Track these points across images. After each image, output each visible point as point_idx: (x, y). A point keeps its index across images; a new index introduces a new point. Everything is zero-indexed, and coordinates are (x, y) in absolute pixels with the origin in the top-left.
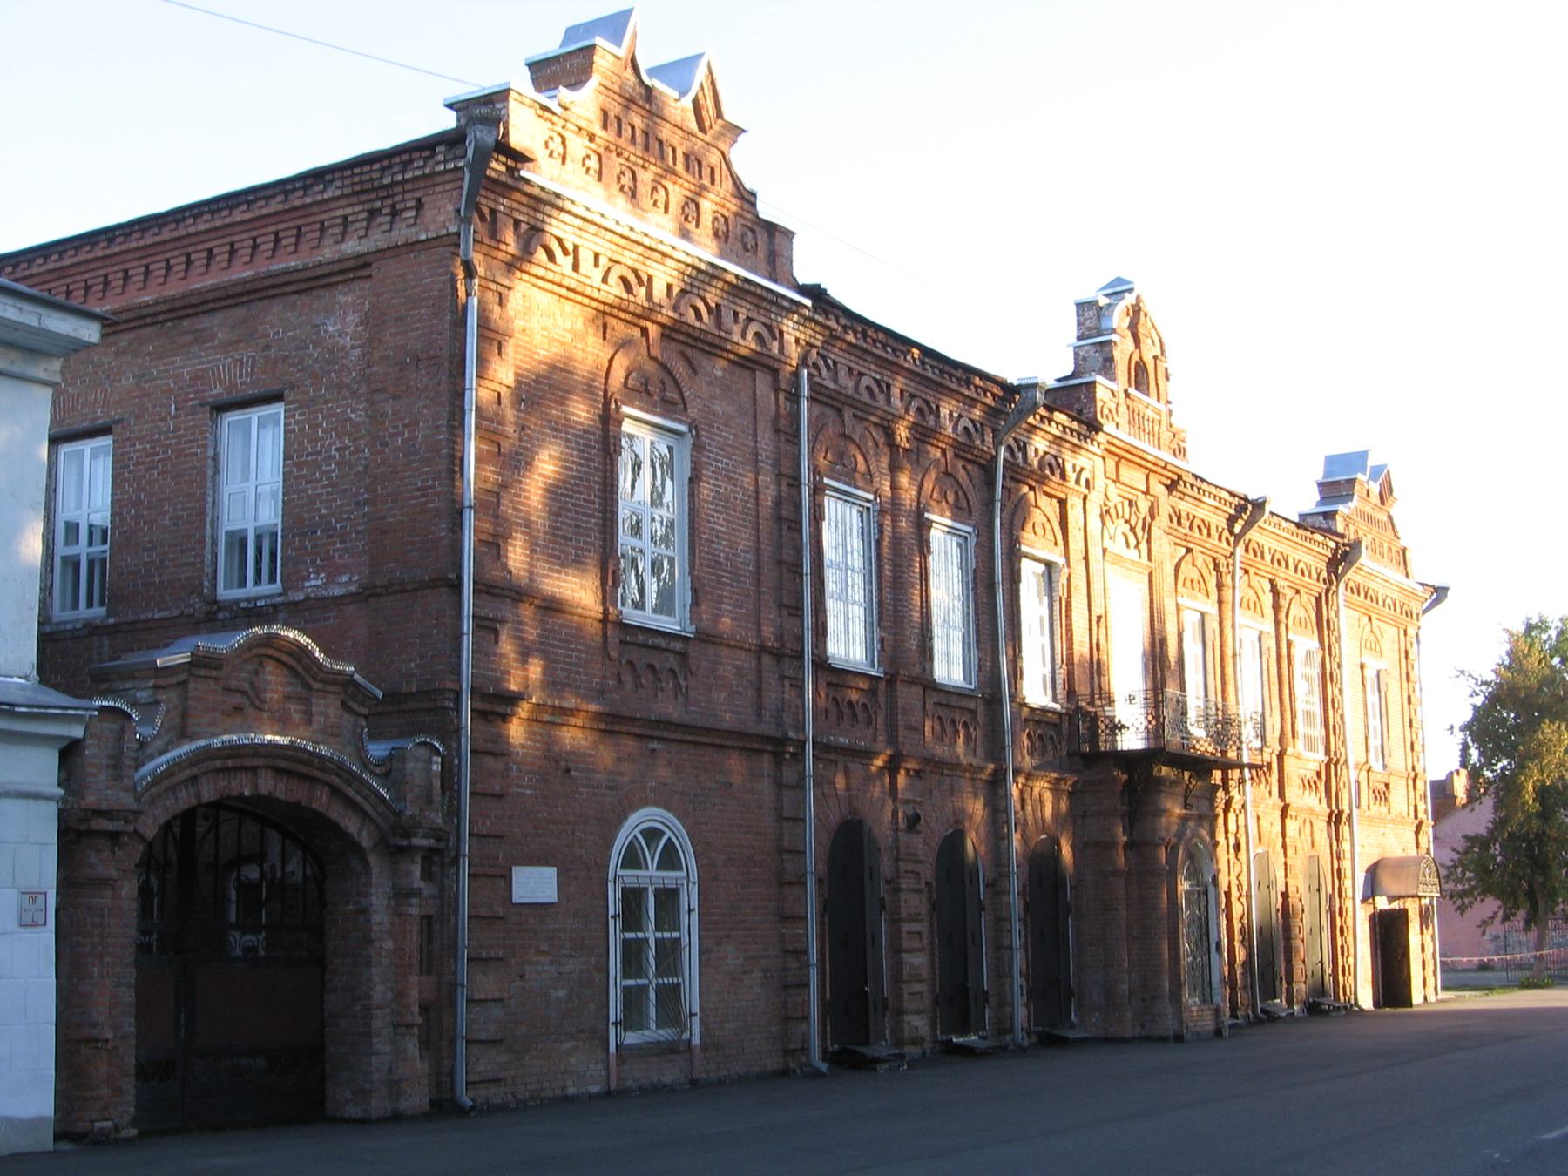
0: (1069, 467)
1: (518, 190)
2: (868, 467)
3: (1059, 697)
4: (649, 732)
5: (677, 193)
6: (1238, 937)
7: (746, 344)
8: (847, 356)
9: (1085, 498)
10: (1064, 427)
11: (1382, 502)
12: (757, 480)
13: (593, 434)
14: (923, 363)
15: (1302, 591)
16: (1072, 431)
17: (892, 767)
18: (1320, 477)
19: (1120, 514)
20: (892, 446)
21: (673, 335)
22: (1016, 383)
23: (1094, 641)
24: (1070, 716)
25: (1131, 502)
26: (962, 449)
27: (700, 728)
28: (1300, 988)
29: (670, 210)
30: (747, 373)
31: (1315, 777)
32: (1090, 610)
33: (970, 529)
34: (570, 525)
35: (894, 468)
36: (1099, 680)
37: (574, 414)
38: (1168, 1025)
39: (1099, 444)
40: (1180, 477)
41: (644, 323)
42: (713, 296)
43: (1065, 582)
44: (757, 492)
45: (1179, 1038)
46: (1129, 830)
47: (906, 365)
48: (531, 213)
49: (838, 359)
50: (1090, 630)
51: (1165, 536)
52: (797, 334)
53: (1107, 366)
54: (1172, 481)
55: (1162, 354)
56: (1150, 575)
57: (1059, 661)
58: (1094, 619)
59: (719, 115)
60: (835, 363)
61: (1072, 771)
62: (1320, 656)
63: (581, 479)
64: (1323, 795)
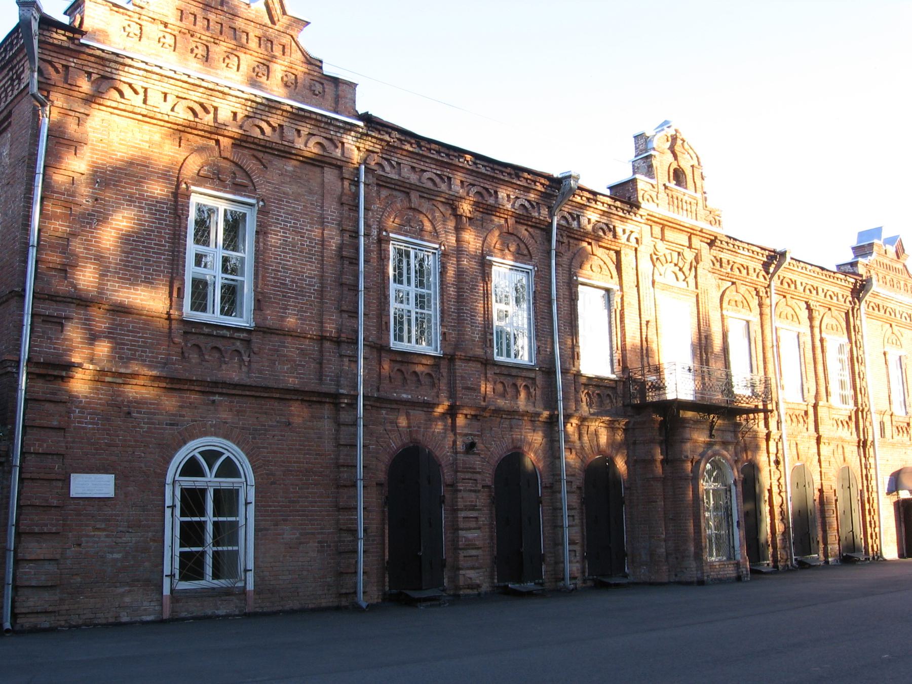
0: (619, 231)
1: (84, 53)
2: (434, 228)
3: (615, 370)
4: (207, 389)
5: (248, 61)
6: (778, 517)
7: (312, 149)
8: (408, 159)
9: (636, 250)
10: (610, 205)
11: (898, 258)
12: (323, 234)
13: (166, 204)
14: (475, 163)
15: (833, 308)
16: (617, 208)
17: (452, 412)
18: (855, 243)
19: (669, 260)
20: (458, 217)
21: (244, 144)
22: (560, 176)
23: (644, 337)
24: (624, 382)
25: (679, 254)
26: (522, 218)
27: (255, 387)
28: (834, 547)
29: (241, 68)
30: (318, 170)
31: (847, 419)
32: (640, 318)
33: (531, 267)
34: (141, 260)
35: (458, 229)
36: (648, 360)
37: (147, 192)
38: (692, 573)
39: (641, 216)
40: (716, 238)
41: (216, 137)
42: (275, 120)
43: (619, 301)
44: (323, 241)
45: (701, 583)
46: (665, 452)
47: (461, 165)
48: (100, 67)
49: (400, 161)
50: (641, 329)
51: (710, 275)
52: (358, 144)
53: (650, 171)
54: (712, 240)
55: (699, 164)
56: (697, 296)
57: (615, 348)
58: (644, 323)
59: (284, 13)
60: (398, 164)
61: (625, 416)
62: (849, 347)
63: (153, 231)
64: (854, 430)
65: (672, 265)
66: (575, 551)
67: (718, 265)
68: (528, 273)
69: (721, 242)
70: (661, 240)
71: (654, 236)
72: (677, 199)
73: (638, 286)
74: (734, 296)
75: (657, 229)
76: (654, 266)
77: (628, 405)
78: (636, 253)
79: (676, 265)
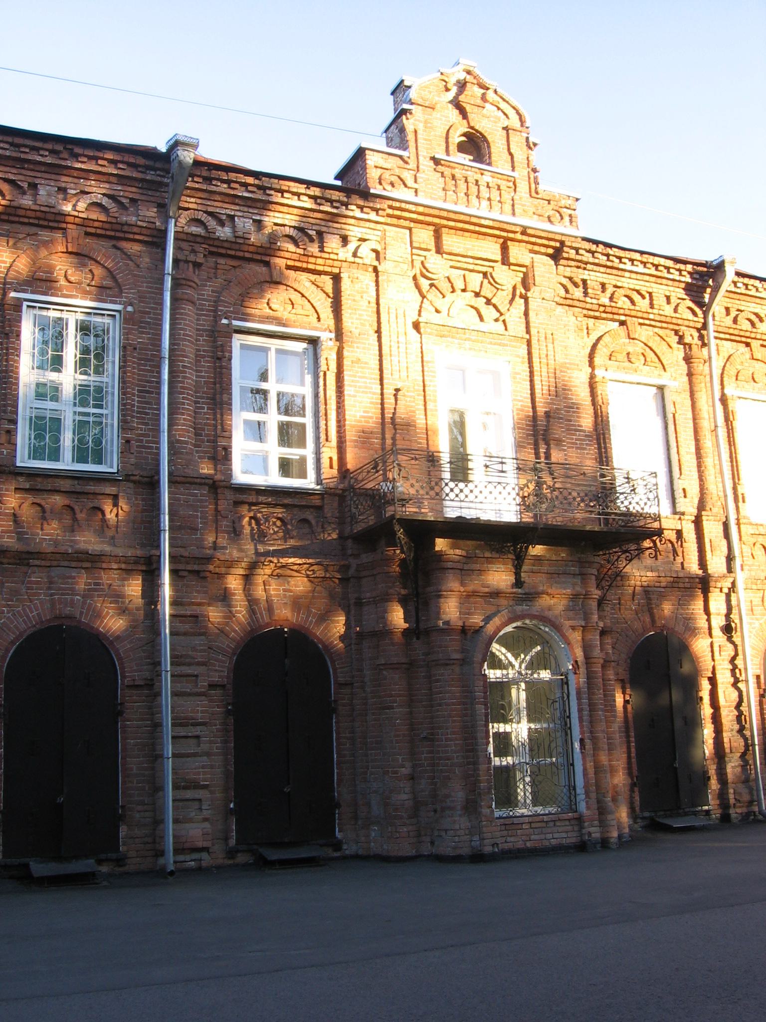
32: (382, 384)
40: (562, 243)
65: (459, 292)
66: (200, 800)
67: (578, 293)
68: (114, 316)
69: (577, 250)
70: (503, 264)
71: (415, 245)
72: (466, 181)
73: (378, 332)
74: (624, 344)
75: (425, 236)
76: (423, 297)
77: (348, 538)
78: (377, 276)
79: (477, 295)
